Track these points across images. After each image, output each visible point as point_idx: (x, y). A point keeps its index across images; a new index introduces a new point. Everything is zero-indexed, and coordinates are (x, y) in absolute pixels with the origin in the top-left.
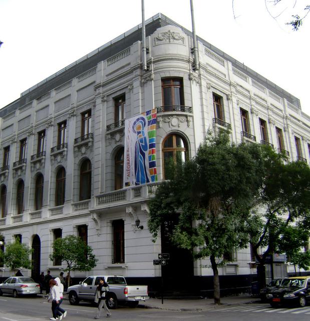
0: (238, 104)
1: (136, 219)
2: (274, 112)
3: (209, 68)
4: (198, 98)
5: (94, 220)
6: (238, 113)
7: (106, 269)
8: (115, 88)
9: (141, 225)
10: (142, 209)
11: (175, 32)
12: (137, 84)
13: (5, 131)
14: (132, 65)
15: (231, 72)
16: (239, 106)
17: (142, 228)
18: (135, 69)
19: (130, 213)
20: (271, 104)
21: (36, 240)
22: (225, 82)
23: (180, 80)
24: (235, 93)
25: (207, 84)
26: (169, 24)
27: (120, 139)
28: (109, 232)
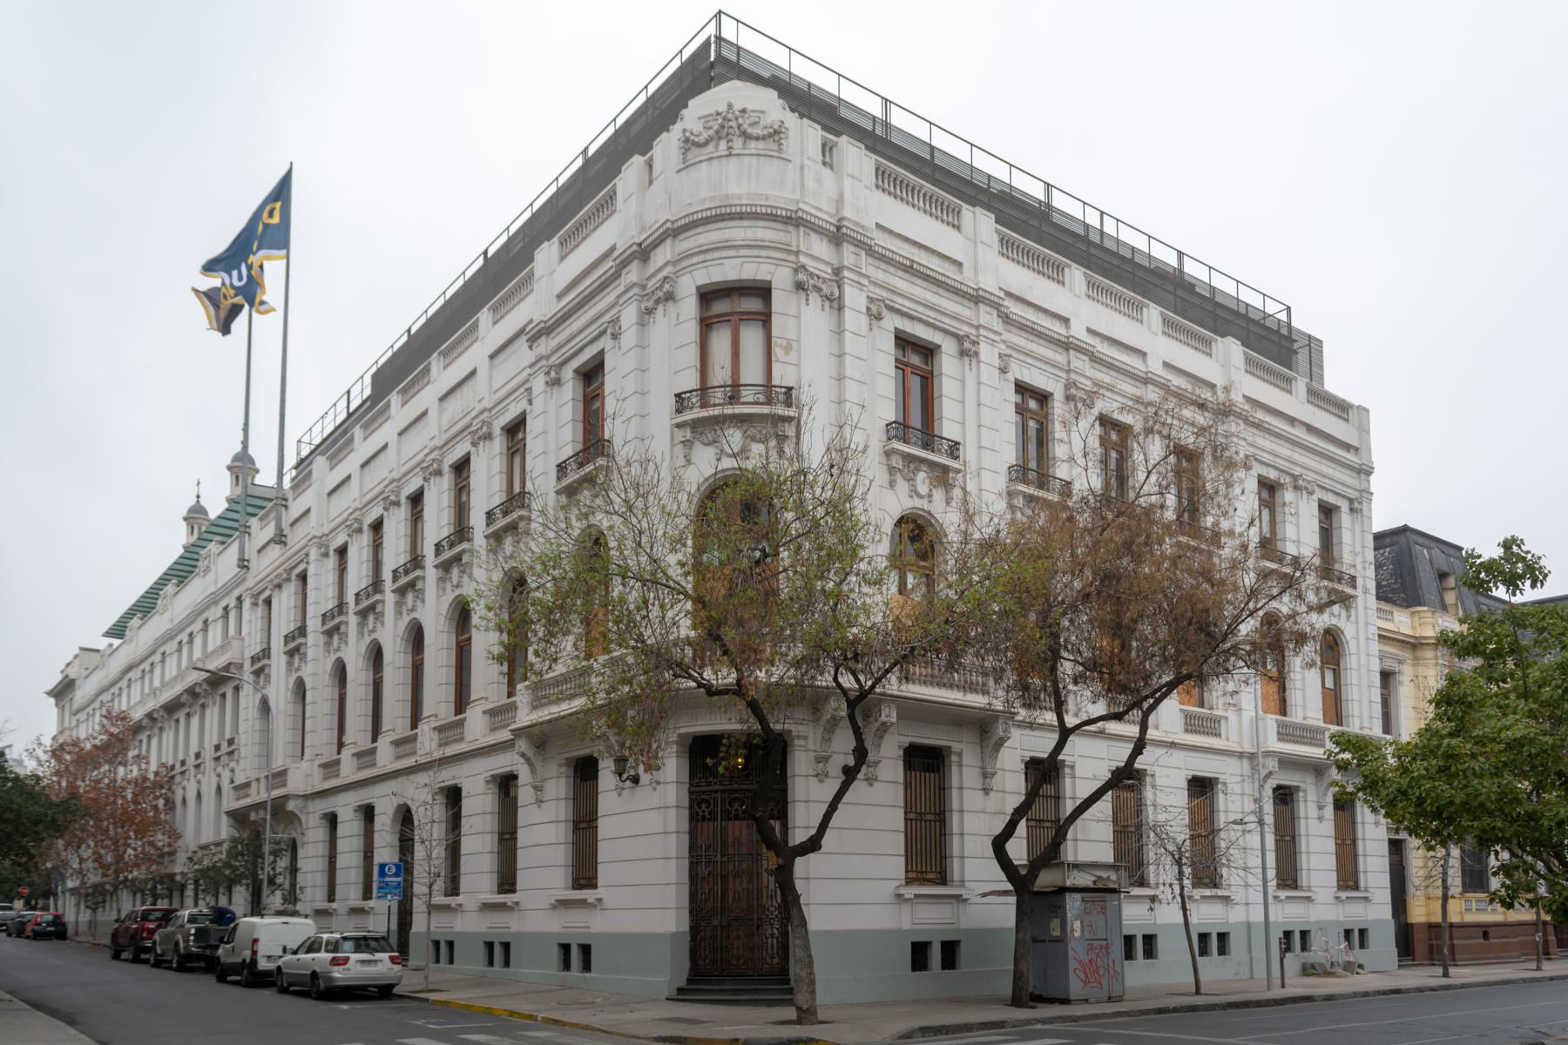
0: (1003, 371)
2: (1095, 359)
3: (882, 240)
11: (750, 107)
13: (335, 497)
20: (1166, 365)
21: (405, 817)
22: (956, 292)
23: (763, 291)
28: (562, 794)
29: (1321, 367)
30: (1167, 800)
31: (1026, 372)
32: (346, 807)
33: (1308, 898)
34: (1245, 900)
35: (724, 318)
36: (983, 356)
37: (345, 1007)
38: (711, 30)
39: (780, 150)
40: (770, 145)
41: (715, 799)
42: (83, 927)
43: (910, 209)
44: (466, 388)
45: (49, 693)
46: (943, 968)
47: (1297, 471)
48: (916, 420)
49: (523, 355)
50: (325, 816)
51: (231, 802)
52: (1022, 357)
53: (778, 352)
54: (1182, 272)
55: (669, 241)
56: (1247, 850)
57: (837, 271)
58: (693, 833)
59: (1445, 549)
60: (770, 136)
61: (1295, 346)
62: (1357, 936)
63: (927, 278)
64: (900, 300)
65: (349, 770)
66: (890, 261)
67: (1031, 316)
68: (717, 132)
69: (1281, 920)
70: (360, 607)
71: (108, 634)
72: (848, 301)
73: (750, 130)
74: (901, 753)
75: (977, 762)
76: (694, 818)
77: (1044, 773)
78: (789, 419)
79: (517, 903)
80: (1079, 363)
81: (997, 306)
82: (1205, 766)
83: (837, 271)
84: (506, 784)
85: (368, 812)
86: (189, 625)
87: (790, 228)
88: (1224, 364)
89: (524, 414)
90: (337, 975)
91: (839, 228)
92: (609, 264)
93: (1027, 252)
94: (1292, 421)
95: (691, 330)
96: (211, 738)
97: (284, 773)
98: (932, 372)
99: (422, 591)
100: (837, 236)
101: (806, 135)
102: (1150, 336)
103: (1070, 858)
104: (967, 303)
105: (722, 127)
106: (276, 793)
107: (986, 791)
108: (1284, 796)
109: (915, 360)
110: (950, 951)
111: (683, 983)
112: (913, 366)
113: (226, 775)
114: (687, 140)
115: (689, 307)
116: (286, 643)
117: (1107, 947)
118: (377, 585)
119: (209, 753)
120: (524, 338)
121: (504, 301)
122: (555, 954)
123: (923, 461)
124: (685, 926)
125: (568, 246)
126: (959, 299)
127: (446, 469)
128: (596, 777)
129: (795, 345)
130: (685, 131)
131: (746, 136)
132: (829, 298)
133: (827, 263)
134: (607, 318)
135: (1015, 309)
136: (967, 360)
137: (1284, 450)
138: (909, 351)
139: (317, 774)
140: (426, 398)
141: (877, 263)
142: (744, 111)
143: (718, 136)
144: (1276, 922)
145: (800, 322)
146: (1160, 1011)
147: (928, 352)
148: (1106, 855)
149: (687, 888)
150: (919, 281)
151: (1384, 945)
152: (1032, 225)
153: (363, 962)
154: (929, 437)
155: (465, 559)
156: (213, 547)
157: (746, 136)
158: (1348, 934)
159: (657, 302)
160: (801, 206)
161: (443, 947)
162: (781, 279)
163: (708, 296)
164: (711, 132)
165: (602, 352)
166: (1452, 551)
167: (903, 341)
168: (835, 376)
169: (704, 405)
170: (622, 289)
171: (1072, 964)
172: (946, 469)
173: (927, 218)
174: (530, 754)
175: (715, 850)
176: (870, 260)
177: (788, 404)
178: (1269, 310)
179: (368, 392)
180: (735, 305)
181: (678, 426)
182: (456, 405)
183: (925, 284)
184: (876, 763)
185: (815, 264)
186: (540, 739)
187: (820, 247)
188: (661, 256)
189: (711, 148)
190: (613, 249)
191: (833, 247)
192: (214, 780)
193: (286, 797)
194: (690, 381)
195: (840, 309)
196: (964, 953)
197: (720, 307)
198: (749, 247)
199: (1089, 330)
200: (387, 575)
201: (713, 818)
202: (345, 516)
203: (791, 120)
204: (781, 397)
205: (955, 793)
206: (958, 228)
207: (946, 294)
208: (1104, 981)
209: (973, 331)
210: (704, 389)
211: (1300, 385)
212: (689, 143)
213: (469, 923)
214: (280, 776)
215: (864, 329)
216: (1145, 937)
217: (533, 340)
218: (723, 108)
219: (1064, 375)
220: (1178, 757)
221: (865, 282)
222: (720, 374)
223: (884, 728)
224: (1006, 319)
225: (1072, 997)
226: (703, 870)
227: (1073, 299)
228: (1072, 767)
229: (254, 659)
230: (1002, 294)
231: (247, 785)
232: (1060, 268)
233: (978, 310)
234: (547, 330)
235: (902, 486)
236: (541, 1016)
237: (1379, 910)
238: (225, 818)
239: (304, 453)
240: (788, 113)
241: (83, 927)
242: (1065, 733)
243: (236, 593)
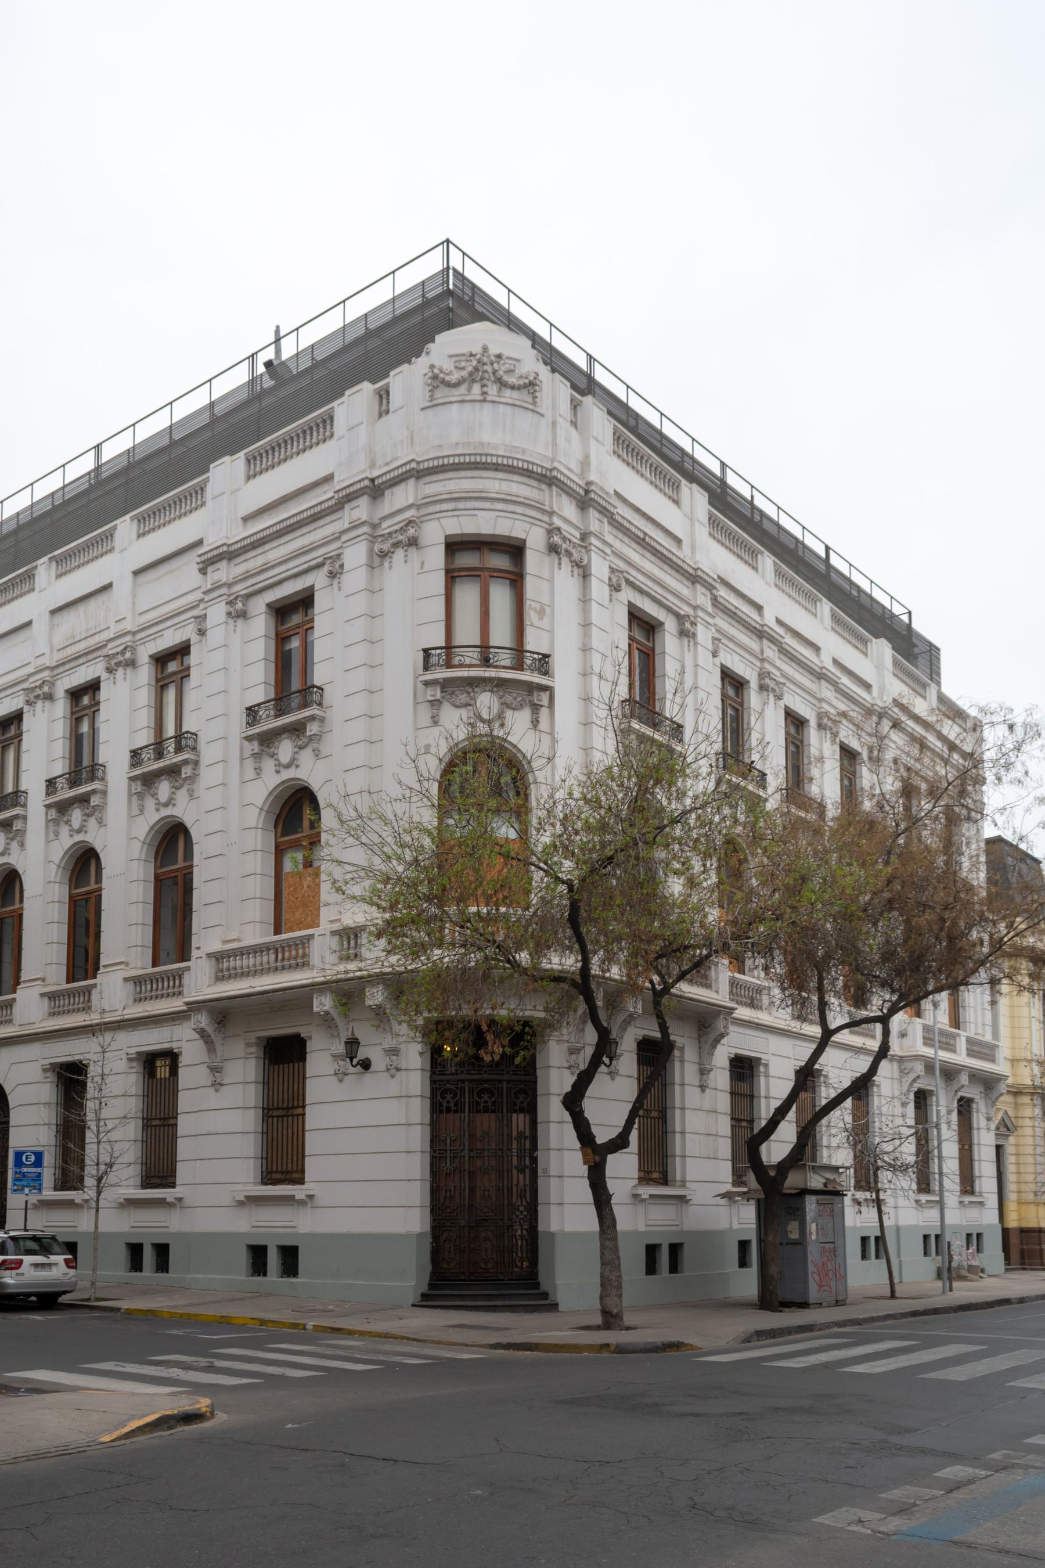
0: (715, 654)
1: (345, 1035)
2: (783, 651)
3: (622, 511)
4: (575, 626)
5: (202, 1033)
6: (711, 685)
7: (240, 1204)
8: (280, 565)
9: (362, 1054)
10: (369, 1002)
11: (506, 353)
12: (355, 555)
14: (343, 479)
15: (702, 532)
16: (717, 661)
17: (366, 1065)
18: (350, 498)
19: (327, 1013)
20: (835, 662)
22: (678, 569)
23: (516, 550)
24: (710, 609)
25: (612, 570)
26: (482, 317)
27: (293, 759)
39: (534, 403)
40: (524, 396)
41: (463, 1089)
44: (93, 604)
49: (186, 578)
53: (531, 616)
55: (411, 482)
58: (435, 1125)
60: (525, 386)
61: (916, 650)
62: (975, 1239)
68: (471, 374)
73: (505, 378)
79: (180, 1200)
83: (584, 536)
87: (544, 487)
90: (9, 1281)
91: (587, 492)
98: (653, 650)
99: (22, 832)
100: (585, 500)
101: (556, 391)
104: (686, 582)
105: (476, 369)
107: (703, 1088)
108: (922, 1098)
110: (290, 1257)
111: (424, 1288)
114: (435, 377)
120: (192, 559)
121: (155, 512)
124: (427, 1228)
125: (256, 468)
126: (679, 577)
127: (60, 692)
128: (303, 1059)
129: (548, 610)
131: (502, 384)
132: (577, 564)
133: (576, 527)
135: (722, 592)
136: (686, 640)
142: (499, 356)
143: (471, 379)
144: (855, 1228)
145: (548, 582)
146: (915, 1314)
149: (428, 1184)
150: (648, 555)
153: (36, 1265)
155: (95, 800)
157: (502, 384)
158: (135, 1251)
159: (396, 545)
160: (556, 464)
162: (535, 540)
163: (454, 546)
164: (464, 373)
169: (449, 665)
171: (811, 1268)
174: (210, 1030)
180: (486, 560)
181: (427, 684)
182: (74, 623)
183: (653, 558)
187: (568, 509)
188: (402, 496)
189: (463, 389)
191: (579, 511)
196: (687, 1256)
197: (467, 560)
198: (505, 501)
201: (459, 1109)
206: (677, 502)
208: (833, 1284)
209: (691, 612)
210: (449, 647)
212: (437, 381)
218: (477, 349)
219: (758, 664)
221: (608, 550)
222: (467, 633)
225: (811, 1301)
228: (766, 1066)
232: (754, 554)
233: (695, 590)
234: (229, 554)
236: (310, 1325)
237: (989, 1217)
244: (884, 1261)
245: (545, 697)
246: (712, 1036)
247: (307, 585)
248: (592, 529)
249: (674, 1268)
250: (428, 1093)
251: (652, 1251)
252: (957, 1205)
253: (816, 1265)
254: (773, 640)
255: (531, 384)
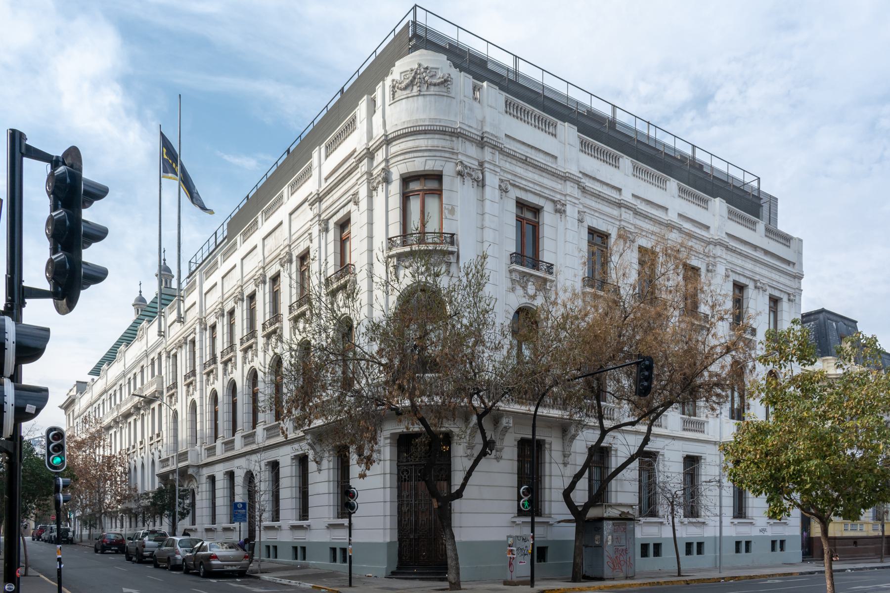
2: (636, 213)
20: (680, 215)
21: (250, 477)
23: (438, 177)
29: (776, 214)
30: (670, 470)
31: (595, 221)
32: (219, 472)
33: (751, 523)
34: (717, 522)
35: (416, 193)
36: (568, 213)
37: (215, 581)
38: (410, 17)
39: (448, 92)
42: (85, 538)
43: (526, 125)
45: (61, 407)
46: (642, 556)
47: (757, 277)
48: (529, 252)
50: (227, 473)
51: (159, 470)
52: (592, 213)
54: (694, 158)
56: (716, 495)
57: (481, 164)
58: (400, 489)
59: (846, 322)
62: (778, 545)
63: (535, 166)
64: (519, 180)
65: (220, 453)
66: (513, 157)
67: (598, 187)
69: (684, 536)
70: (224, 360)
71: (90, 373)
72: (488, 181)
74: (516, 443)
75: (560, 448)
76: (400, 480)
77: (599, 455)
78: (452, 253)
80: (627, 216)
81: (578, 183)
82: (694, 449)
83: (481, 164)
84: (302, 461)
85: (231, 475)
86: (133, 368)
87: (454, 139)
88: (716, 214)
89: (308, 248)
91: (482, 138)
92: (352, 160)
93: (597, 149)
94: (755, 247)
95: (395, 201)
96: (148, 433)
97: (186, 453)
98: (538, 223)
100: (482, 143)
101: (463, 81)
102: (670, 197)
103: (613, 501)
104: (560, 181)
106: (181, 465)
107: (565, 464)
109: (529, 215)
112: (527, 220)
113: (157, 454)
115: (395, 187)
116: (185, 380)
117: (626, 550)
118: (232, 347)
119: (147, 442)
120: (307, 204)
122: (328, 553)
123: (532, 275)
124: (396, 539)
125: (330, 149)
130: (393, 80)
132: (476, 180)
134: (351, 192)
135: (588, 183)
137: (749, 265)
138: (525, 210)
139: (204, 453)
140: (256, 238)
141: (505, 158)
142: (427, 68)
145: (458, 193)
147: (537, 210)
148: (633, 499)
150: (531, 169)
151: (795, 550)
152: (603, 133)
154: (535, 263)
156: (144, 324)
161: (299, 549)
162: (449, 170)
163: (406, 180)
165: (349, 213)
166: (850, 323)
167: (521, 204)
168: (479, 226)
170: (359, 175)
171: (606, 559)
172: (545, 280)
173: (537, 130)
175: (411, 497)
176: (501, 156)
177: (452, 243)
178: (747, 181)
179: (225, 234)
181: (389, 257)
183: (534, 170)
184: (501, 450)
185: (469, 160)
186: (319, 436)
187: (472, 150)
190: (355, 151)
191: (479, 150)
192: (151, 456)
193: (188, 467)
194: (395, 230)
195: (483, 186)
196: (753, 546)
197: (414, 186)
199: (633, 195)
200: (237, 341)
202: (214, 306)
203: (454, 72)
204: (448, 240)
205: (547, 465)
207: (547, 176)
210: (405, 233)
211: (761, 226)
213: (285, 537)
214: (183, 456)
215: (497, 198)
216: (655, 544)
217: (312, 204)
219: (618, 223)
220: (678, 444)
221: (498, 170)
223: (506, 429)
224: (584, 190)
225: (605, 577)
226: (405, 509)
227: (624, 177)
228: (616, 450)
229: (169, 389)
230: (580, 175)
231: (168, 459)
232: (617, 159)
234: (319, 199)
235: (520, 291)
238: (157, 478)
239: (193, 269)
240: (453, 68)
241: (85, 538)
242: (604, 432)
243: (158, 350)
244: (347, 564)
245: (453, 259)
246: (569, 436)
247: (345, 212)
248: (487, 159)
249: (747, 550)
250: (396, 472)
251: (738, 543)
252: (729, 524)
253: (610, 558)
254: (628, 208)
255: (446, 81)
